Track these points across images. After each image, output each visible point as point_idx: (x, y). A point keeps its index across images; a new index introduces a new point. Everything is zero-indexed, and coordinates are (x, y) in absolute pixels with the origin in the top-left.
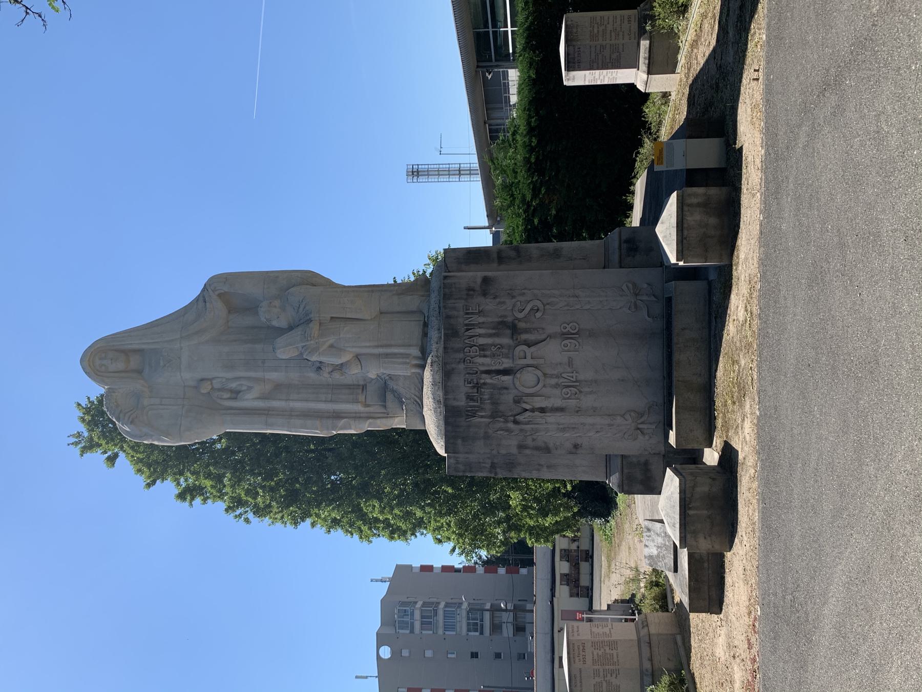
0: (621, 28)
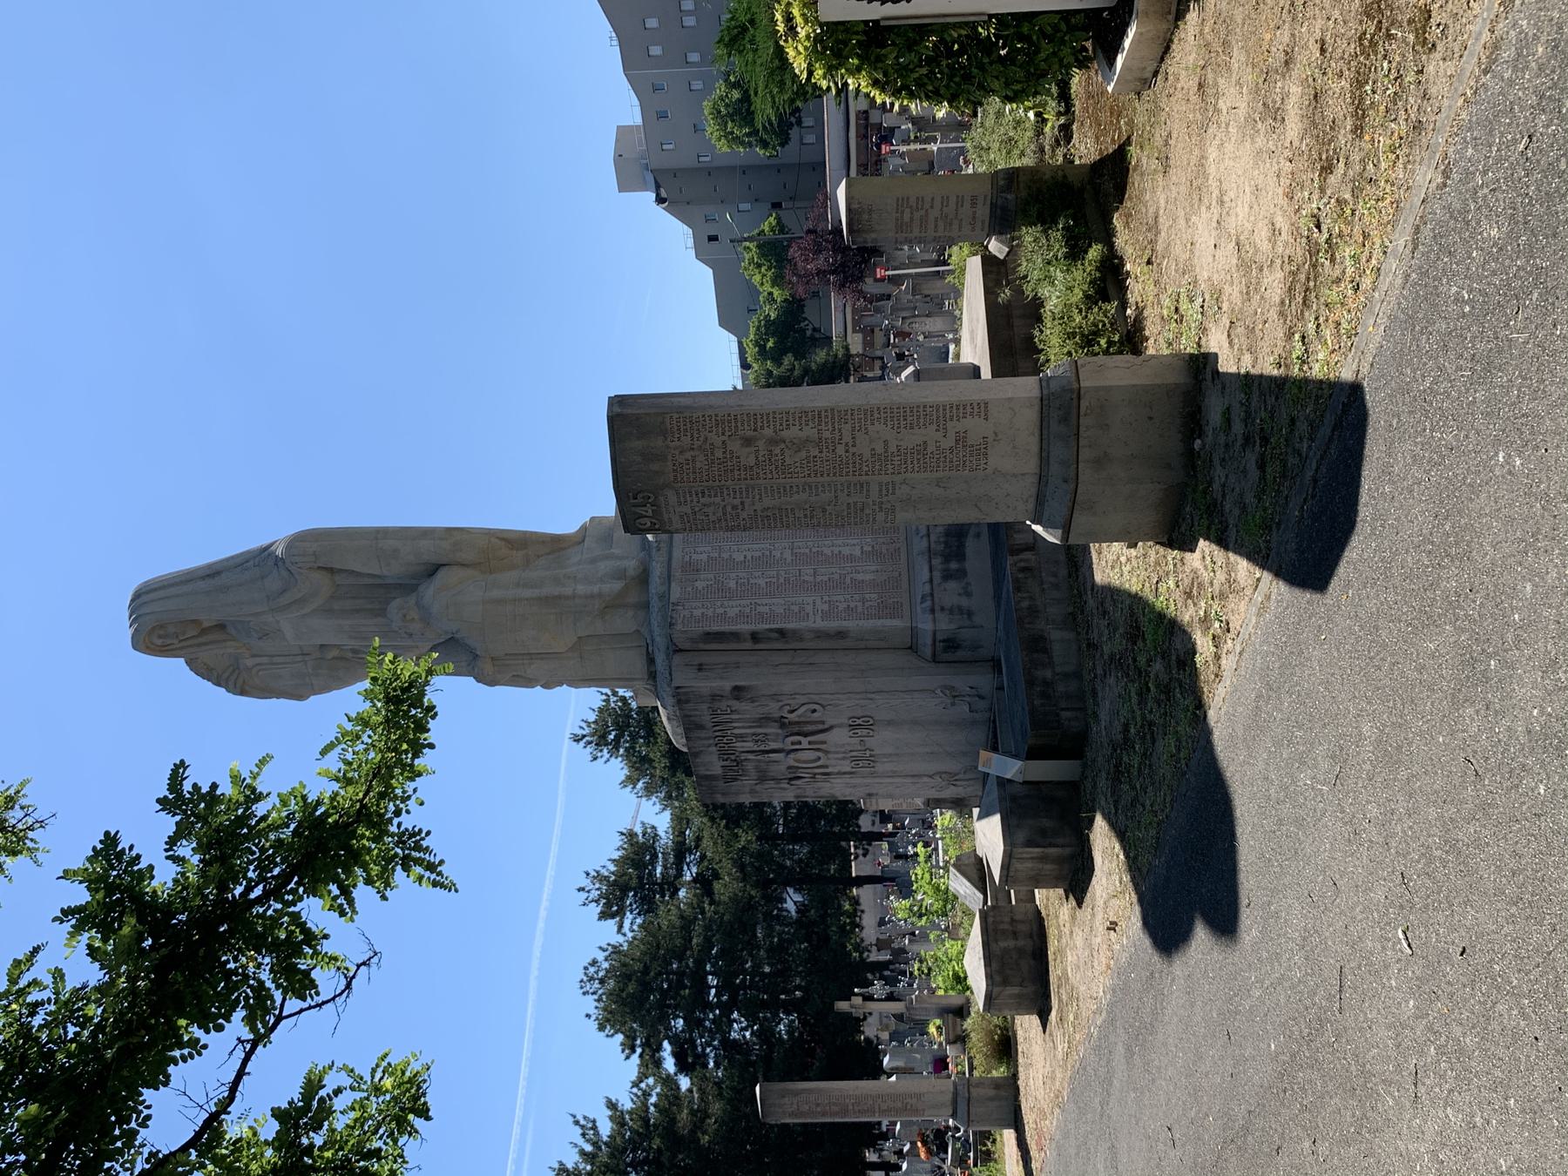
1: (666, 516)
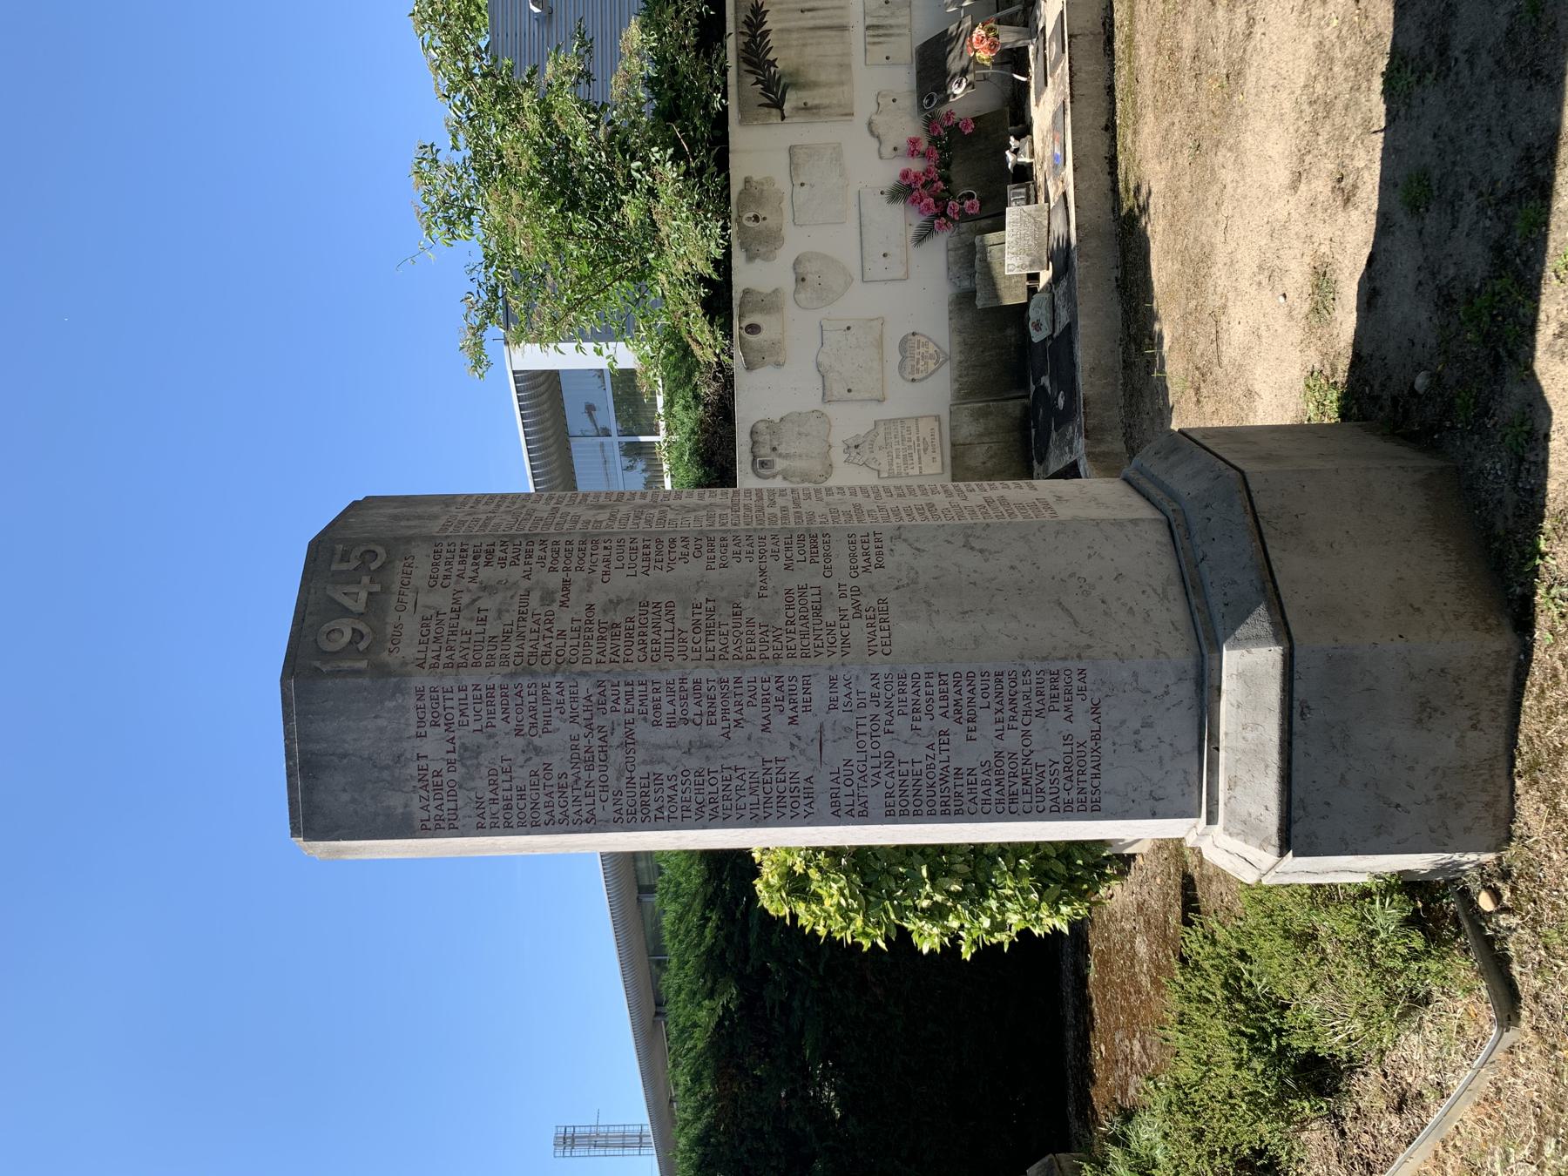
1: (392, 618)
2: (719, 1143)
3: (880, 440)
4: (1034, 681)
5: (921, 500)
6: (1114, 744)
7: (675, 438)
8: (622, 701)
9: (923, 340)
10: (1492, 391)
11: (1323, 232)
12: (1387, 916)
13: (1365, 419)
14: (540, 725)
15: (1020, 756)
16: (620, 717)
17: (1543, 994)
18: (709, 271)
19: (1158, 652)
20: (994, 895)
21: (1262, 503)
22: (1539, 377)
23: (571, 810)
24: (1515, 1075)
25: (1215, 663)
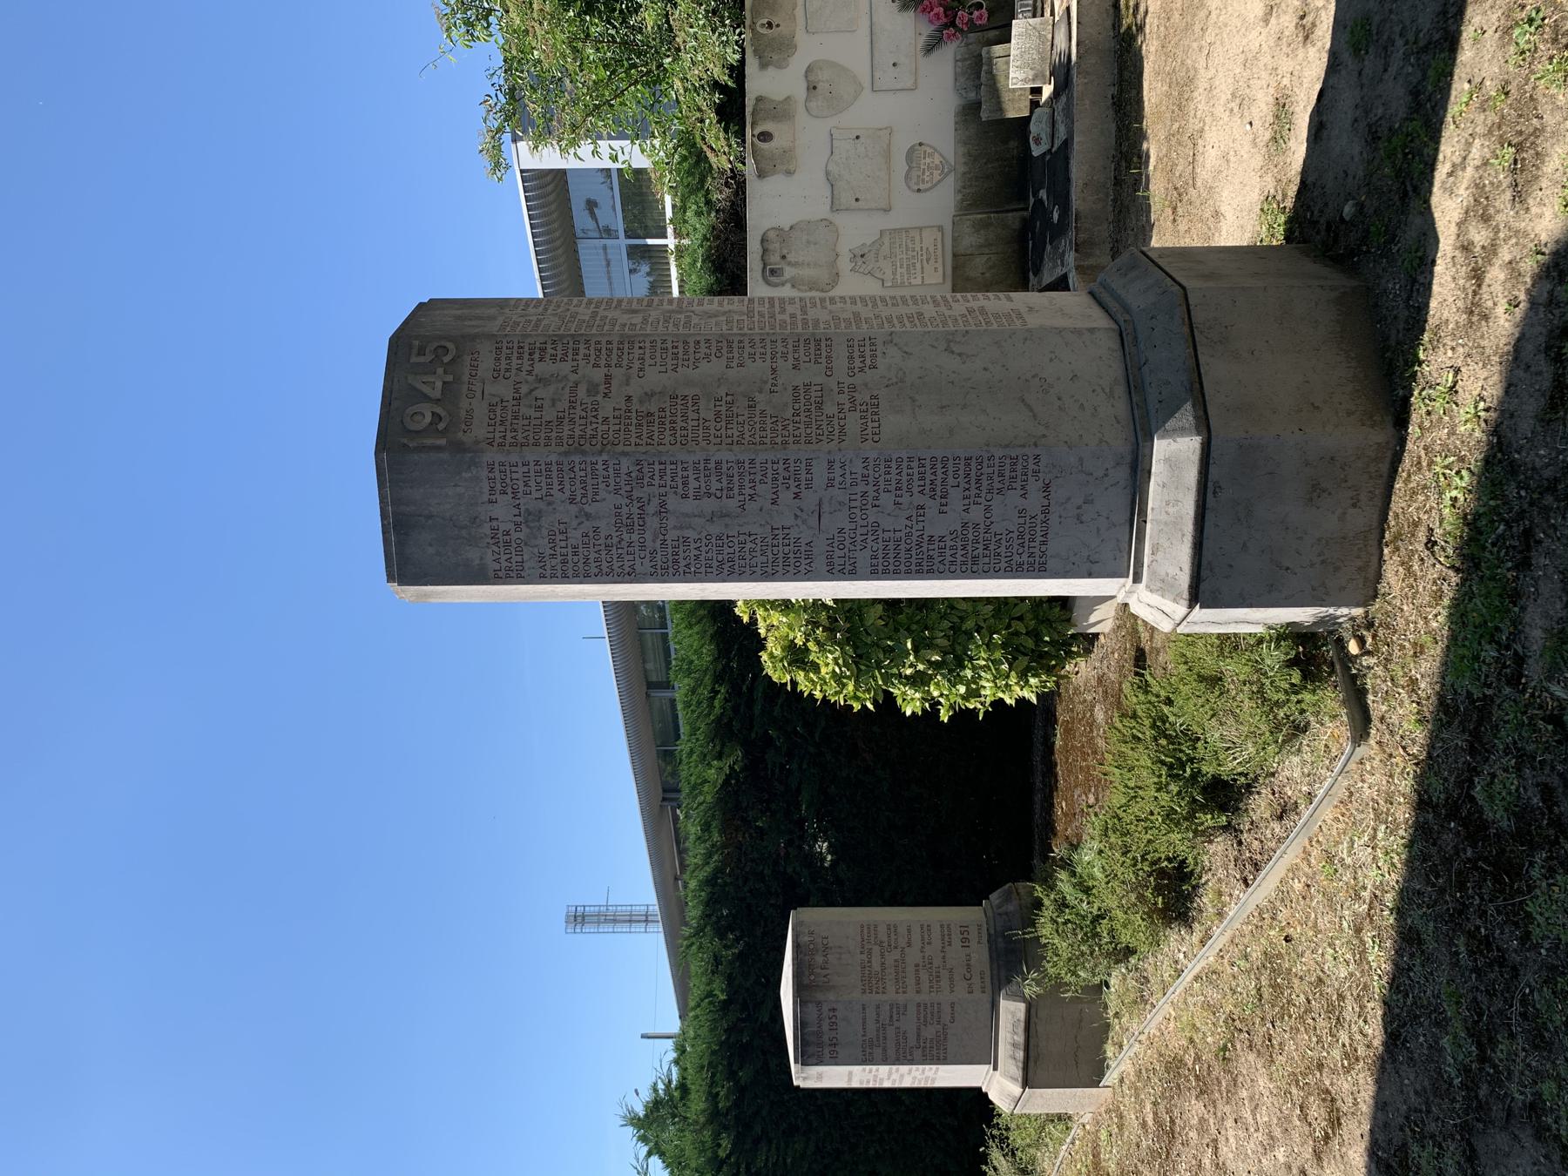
0: (944, 957)
1: (464, 404)
2: (726, 884)
3: (885, 249)
4: (997, 465)
5: (912, 309)
6: (1060, 517)
7: (686, 242)
8: (657, 477)
9: (929, 150)
10: (1399, 222)
11: (1286, 65)
12: (1273, 658)
13: (1305, 242)
14: (590, 496)
15: (982, 526)
16: (656, 490)
17: (1387, 716)
18: (724, 78)
19: (1101, 441)
20: (970, 666)
21: (1199, 316)
22: (1434, 210)
23: (616, 565)
24: (1363, 781)
25: (1147, 451)
